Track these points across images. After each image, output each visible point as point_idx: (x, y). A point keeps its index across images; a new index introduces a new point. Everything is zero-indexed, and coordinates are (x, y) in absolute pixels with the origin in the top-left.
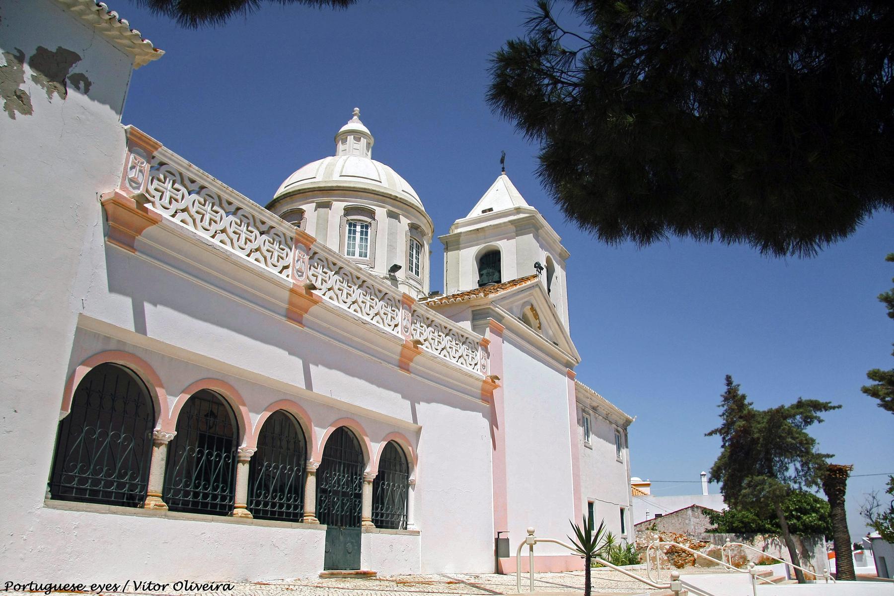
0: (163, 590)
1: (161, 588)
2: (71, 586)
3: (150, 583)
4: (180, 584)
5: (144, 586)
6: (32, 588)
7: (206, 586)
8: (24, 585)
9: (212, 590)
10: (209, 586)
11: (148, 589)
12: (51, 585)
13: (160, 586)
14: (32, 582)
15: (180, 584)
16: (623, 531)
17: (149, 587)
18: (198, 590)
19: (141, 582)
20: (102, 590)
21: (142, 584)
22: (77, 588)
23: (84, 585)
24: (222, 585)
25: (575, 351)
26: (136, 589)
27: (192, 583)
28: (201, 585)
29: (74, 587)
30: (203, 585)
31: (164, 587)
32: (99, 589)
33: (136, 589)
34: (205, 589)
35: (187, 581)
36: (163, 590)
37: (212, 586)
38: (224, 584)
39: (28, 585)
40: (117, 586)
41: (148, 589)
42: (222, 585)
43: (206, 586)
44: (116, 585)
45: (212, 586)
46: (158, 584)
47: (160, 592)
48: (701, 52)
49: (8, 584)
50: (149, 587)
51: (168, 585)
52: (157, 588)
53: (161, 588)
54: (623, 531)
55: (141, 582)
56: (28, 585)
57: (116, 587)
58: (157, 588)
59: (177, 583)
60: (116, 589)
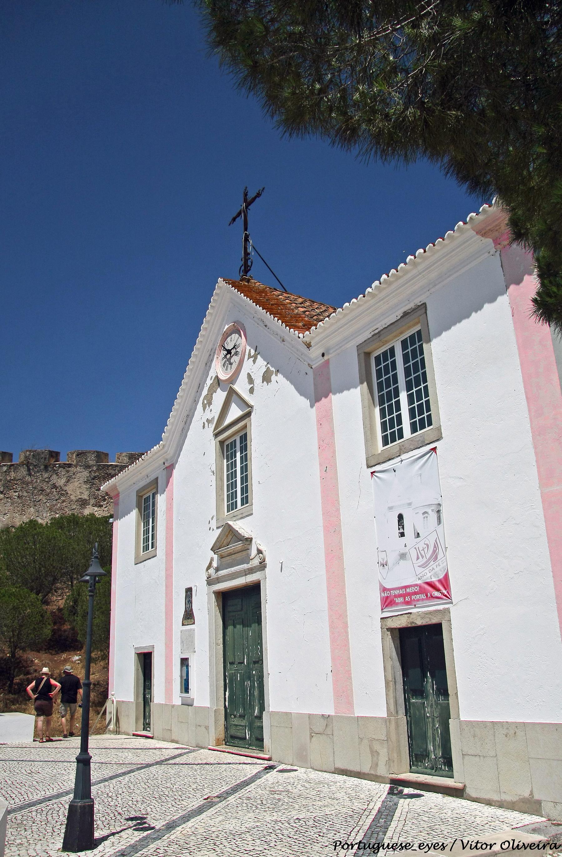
0: (490, 849)
1: (489, 847)
2: (398, 845)
3: (477, 842)
4: (507, 844)
5: (471, 845)
6: (360, 847)
7: (437, 845)
8: (491, 844)
9: (538, 849)
10: (440, 844)
11: (368, 849)
12: (379, 844)
13: (487, 845)
14: (478, 841)
15: (507, 844)
16: (246, 229)
17: (476, 846)
18: (525, 849)
19: (468, 841)
20: (429, 849)
21: (470, 843)
22: (405, 847)
23: (411, 845)
24: (549, 844)
25: (434, 602)
26: (464, 848)
27: (519, 842)
28: (432, 844)
29: (402, 846)
30: (434, 844)
31: (491, 846)
32: (427, 849)
33: (464, 848)
34: (436, 848)
35: (514, 840)
36: (490, 849)
37: (538, 845)
38: (551, 842)
39: (356, 844)
40: (445, 845)
41: (368, 849)
42: (549, 844)
43: (437, 845)
44: (443, 844)
45: (538, 845)
46: (485, 843)
47: (488, 850)
48: (43, 569)
49: (336, 843)
50: (476, 846)
51: (495, 844)
52: (484, 846)
53: (489, 847)
54: (246, 229)
55: (468, 841)
56: (356, 844)
57: (443, 846)
58: (484, 846)
59: (504, 842)
60: (444, 848)
